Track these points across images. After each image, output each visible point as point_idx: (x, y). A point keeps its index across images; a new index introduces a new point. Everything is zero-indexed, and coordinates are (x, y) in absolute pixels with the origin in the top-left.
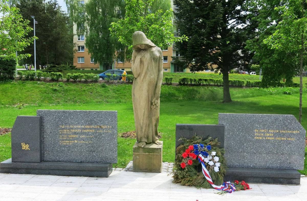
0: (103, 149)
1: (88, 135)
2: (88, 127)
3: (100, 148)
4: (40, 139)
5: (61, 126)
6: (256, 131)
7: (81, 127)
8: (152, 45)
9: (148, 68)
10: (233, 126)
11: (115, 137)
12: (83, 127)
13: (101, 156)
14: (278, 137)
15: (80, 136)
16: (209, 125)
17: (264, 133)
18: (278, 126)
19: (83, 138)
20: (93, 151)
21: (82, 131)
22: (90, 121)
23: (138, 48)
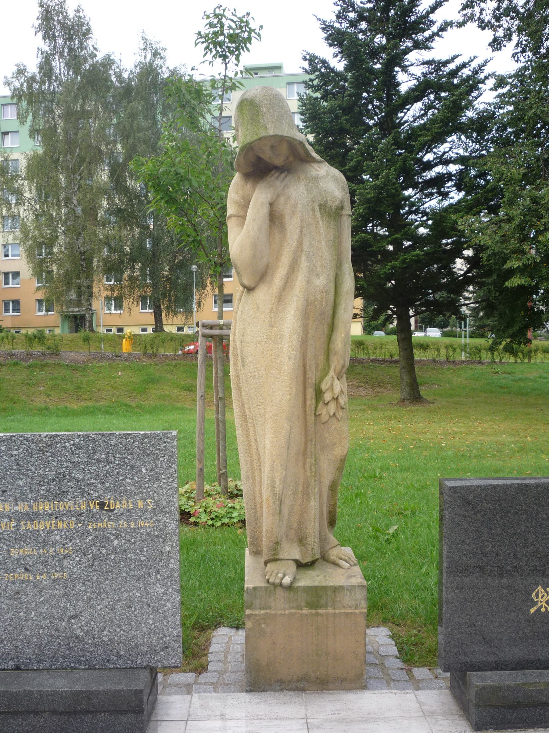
0: (118, 606)
1: (45, 544)
2: (46, 507)
3: (105, 603)
7: (16, 508)
9: (300, 243)
11: (168, 549)
13: (106, 639)
15: (9, 551)
16: (476, 483)
20: (72, 617)
21: (17, 527)
22: (54, 480)
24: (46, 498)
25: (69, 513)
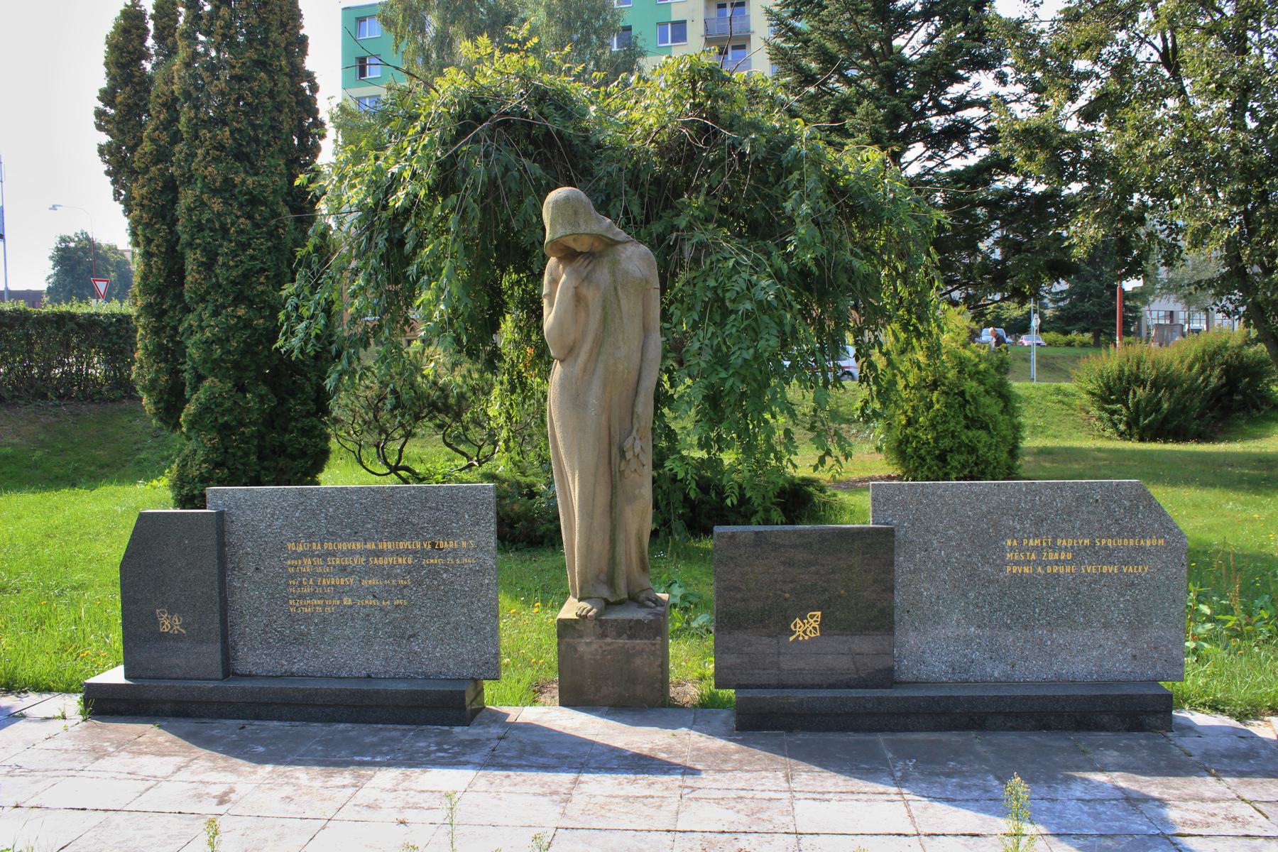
1: (389, 576)
3: (437, 625)
4: (220, 594)
5: (291, 546)
6: (1009, 543)
8: (619, 238)
10: (927, 530)
12: (371, 546)
14: (1090, 564)
17: (1038, 550)
18: (1089, 522)
19: (373, 586)
20: (411, 636)
21: (367, 561)
23: (568, 248)
24: (389, 539)
25: (407, 552)
